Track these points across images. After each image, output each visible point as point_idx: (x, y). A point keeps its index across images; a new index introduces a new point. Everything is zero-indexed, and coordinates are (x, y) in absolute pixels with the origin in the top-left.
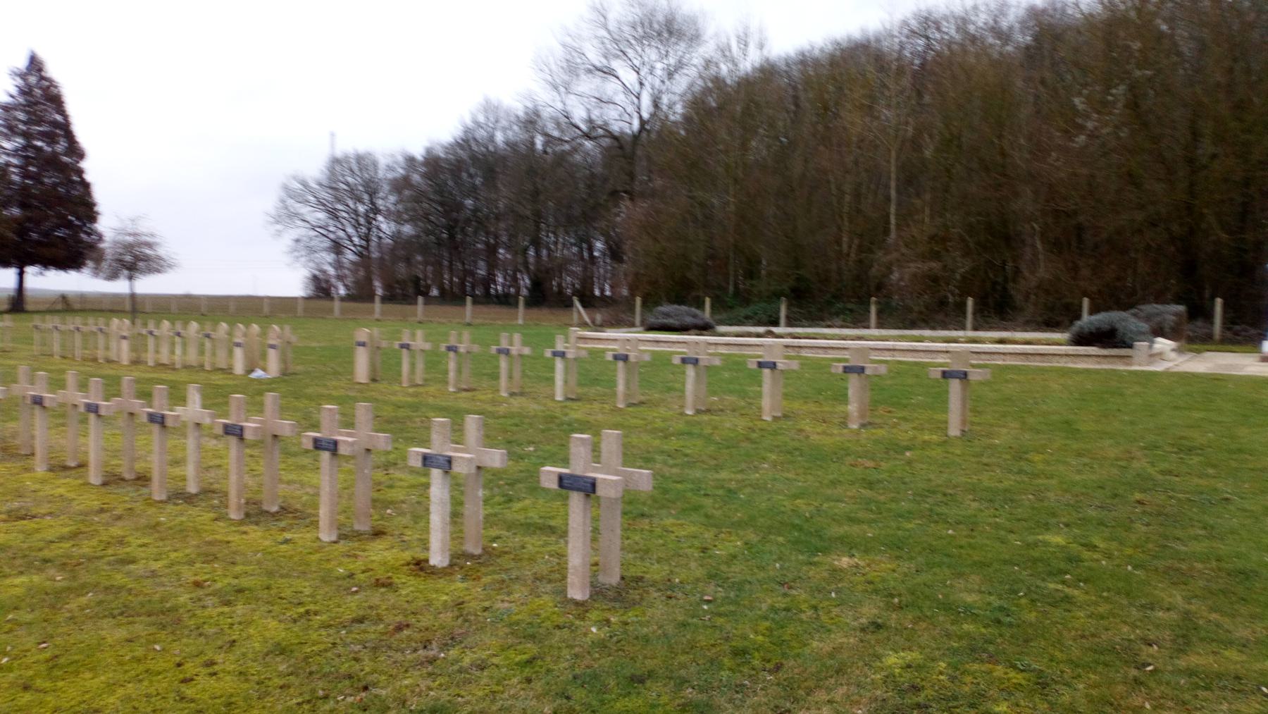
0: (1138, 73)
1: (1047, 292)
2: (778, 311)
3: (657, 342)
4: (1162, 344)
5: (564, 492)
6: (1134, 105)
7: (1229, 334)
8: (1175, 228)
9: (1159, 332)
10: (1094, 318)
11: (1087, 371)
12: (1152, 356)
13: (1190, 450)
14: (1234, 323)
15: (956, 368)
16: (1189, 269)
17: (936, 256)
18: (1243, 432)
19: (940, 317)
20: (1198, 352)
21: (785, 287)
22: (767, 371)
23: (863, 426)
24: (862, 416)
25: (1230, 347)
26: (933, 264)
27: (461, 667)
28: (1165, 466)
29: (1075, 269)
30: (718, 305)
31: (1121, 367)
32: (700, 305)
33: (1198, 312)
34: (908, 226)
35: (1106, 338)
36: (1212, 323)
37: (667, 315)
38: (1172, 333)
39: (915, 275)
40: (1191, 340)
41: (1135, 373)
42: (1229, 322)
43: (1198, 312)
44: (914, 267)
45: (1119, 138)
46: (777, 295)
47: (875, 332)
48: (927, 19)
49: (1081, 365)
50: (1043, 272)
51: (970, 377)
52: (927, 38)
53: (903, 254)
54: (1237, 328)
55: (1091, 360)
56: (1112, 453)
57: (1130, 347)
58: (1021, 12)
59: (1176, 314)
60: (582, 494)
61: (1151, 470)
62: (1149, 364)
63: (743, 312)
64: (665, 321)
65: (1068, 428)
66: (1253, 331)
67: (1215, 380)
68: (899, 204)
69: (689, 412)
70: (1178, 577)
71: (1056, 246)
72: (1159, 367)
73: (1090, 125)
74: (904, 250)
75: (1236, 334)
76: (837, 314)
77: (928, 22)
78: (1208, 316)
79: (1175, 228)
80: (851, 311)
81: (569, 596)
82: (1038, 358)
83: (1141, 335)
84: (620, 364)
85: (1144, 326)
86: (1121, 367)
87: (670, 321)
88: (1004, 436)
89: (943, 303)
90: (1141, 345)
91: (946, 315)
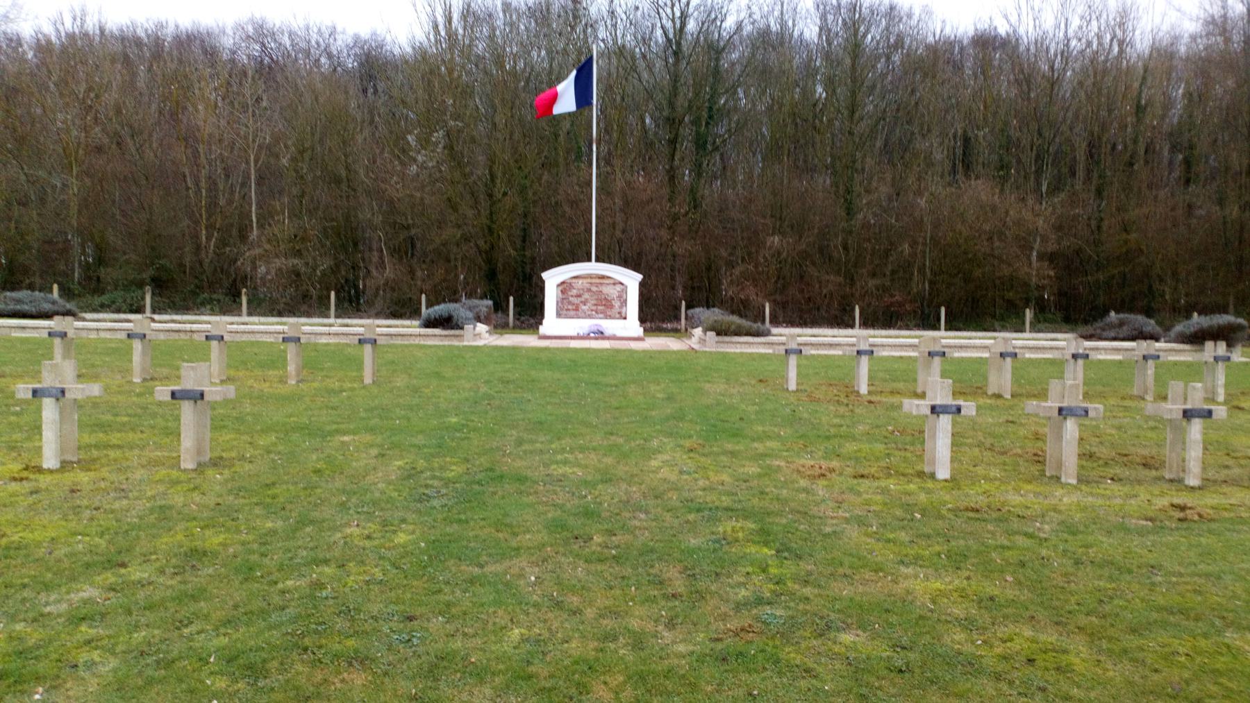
0: (452, 123)
1: (393, 290)
2: (143, 299)
3: (24, 328)
4: (482, 328)
5: (174, 402)
6: (450, 147)
7: (518, 323)
8: (481, 243)
9: (478, 319)
10: (431, 310)
11: (435, 346)
12: (475, 335)
13: (508, 382)
14: (520, 315)
15: (367, 336)
16: (491, 275)
17: (298, 254)
18: (533, 373)
19: (304, 308)
20: (501, 334)
21: (146, 276)
22: (214, 343)
23: (298, 382)
24: (298, 375)
25: (518, 331)
26: (296, 261)
27: (847, 108)
28: (497, 389)
29: (412, 272)
30: (66, 292)
31: (456, 343)
32: (51, 291)
33: (500, 307)
34: (270, 225)
35: (445, 322)
36: (508, 315)
37: (19, 301)
38: (486, 321)
39: (280, 269)
40: (496, 327)
41: (466, 346)
42: (518, 314)
43: (500, 307)
44: (278, 263)
45: (440, 171)
46: (141, 285)
47: (245, 319)
48: (261, 27)
49: (430, 342)
50: (389, 272)
51: (378, 342)
52: (263, 45)
53: (266, 251)
54: (523, 318)
55: (437, 338)
56: (467, 386)
57: (462, 328)
58: (350, 41)
59: (487, 307)
60: (192, 402)
61: (489, 391)
62: (474, 340)
63: (97, 300)
64: (18, 307)
65: (438, 375)
66: (532, 321)
67: (514, 350)
68: (259, 206)
69: (137, 380)
70: (513, 427)
71: (396, 251)
72: (480, 343)
73: (420, 158)
74: (268, 247)
75: (523, 322)
76: (203, 304)
77: (261, 33)
78: (506, 311)
79: (481, 243)
80: (219, 301)
81: (545, 275)
82: (400, 338)
83: (468, 320)
84: (57, 341)
85: (470, 315)
86: (456, 343)
87: (26, 308)
88: (400, 381)
89: (306, 297)
90: (468, 327)
91: (310, 306)
